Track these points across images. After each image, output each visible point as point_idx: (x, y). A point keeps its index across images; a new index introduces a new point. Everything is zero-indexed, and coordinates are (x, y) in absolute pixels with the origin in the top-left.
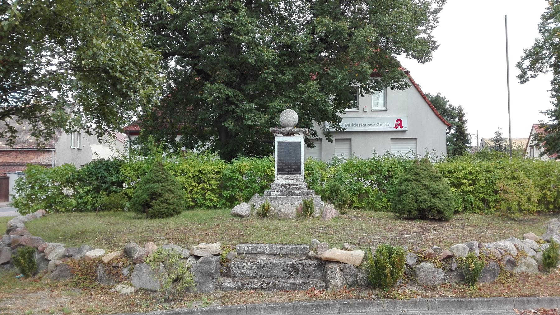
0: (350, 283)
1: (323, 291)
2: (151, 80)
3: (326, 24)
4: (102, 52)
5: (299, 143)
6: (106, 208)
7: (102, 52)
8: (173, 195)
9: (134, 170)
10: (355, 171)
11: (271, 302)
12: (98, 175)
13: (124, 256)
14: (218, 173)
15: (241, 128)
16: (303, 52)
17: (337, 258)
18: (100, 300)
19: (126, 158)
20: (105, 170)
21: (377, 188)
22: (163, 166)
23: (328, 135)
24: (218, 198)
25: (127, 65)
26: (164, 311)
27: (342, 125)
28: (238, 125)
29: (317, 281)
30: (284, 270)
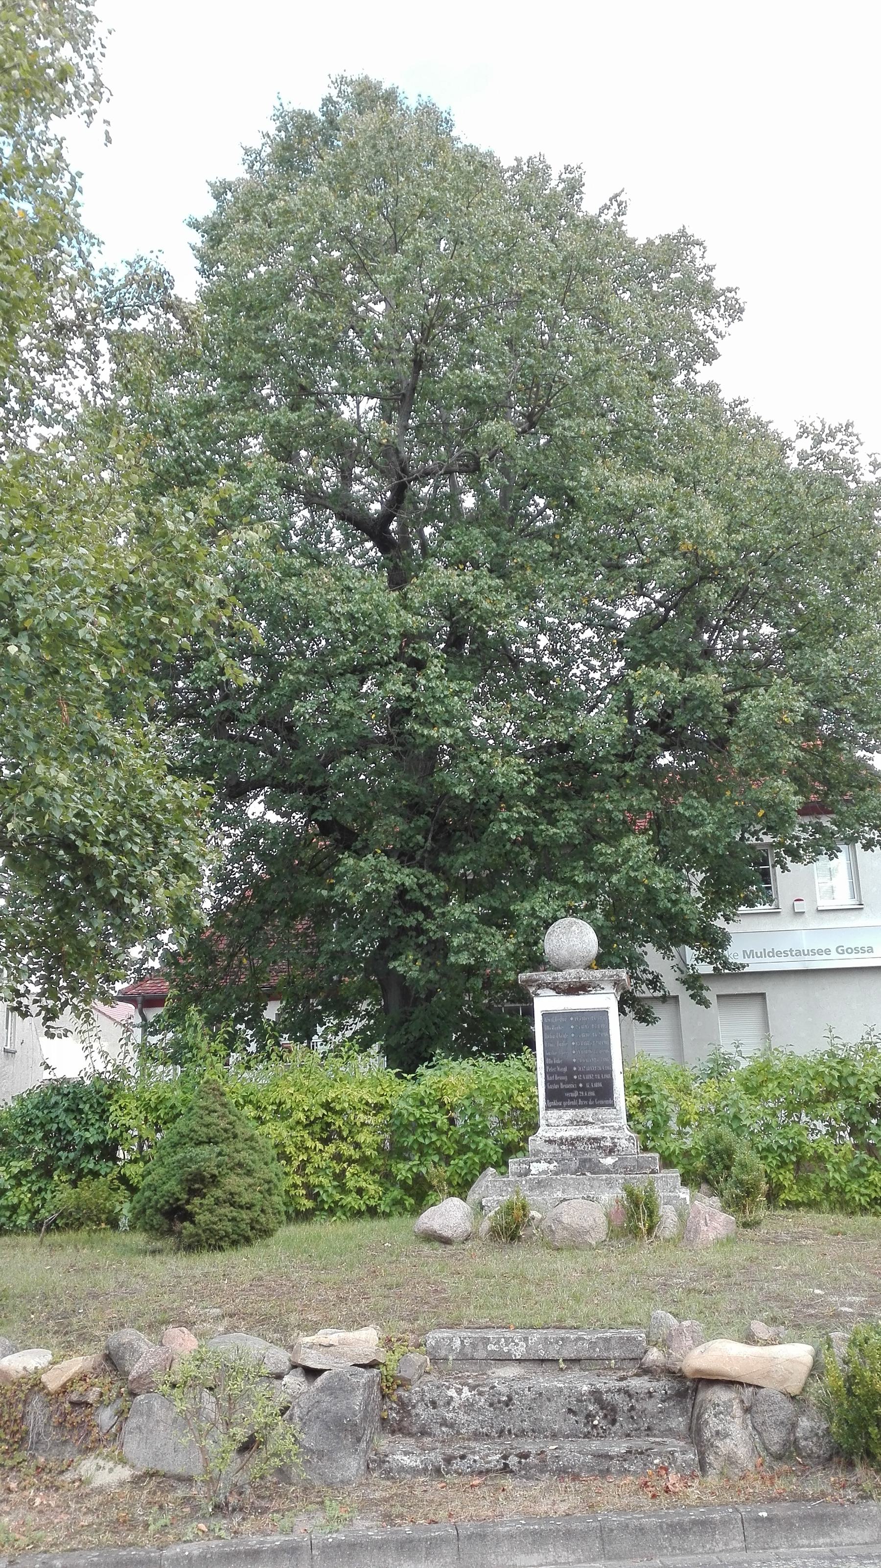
0: (774, 1449)
1: (693, 1476)
2: (186, 861)
3: (663, 683)
4: (58, 797)
5: (604, 1013)
6: (70, 1221)
7: (58, 797)
8: (250, 1180)
9: (148, 1108)
10: (778, 1092)
11: (530, 1517)
12: (48, 1127)
13: (104, 1370)
14: (379, 1108)
15: (444, 975)
16: (605, 759)
17: (732, 1370)
18: (31, 1508)
19: (125, 1076)
20: (67, 1110)
21: (850, 1141)
22: (223, 1094)
23: (694, 984)
24: (381, 1184)
25: (122, 825)
26: (213, 1544)
27: (734, 953)
28: (433, 965)
29: (675, 1445)
30: (570, 1411)
